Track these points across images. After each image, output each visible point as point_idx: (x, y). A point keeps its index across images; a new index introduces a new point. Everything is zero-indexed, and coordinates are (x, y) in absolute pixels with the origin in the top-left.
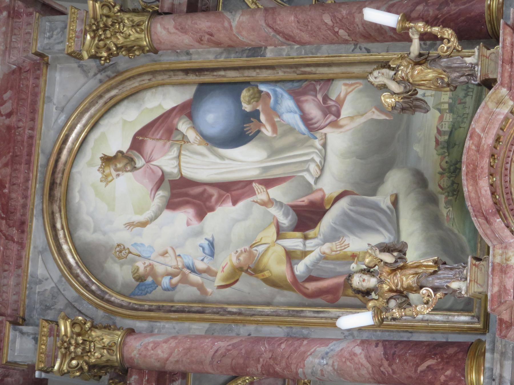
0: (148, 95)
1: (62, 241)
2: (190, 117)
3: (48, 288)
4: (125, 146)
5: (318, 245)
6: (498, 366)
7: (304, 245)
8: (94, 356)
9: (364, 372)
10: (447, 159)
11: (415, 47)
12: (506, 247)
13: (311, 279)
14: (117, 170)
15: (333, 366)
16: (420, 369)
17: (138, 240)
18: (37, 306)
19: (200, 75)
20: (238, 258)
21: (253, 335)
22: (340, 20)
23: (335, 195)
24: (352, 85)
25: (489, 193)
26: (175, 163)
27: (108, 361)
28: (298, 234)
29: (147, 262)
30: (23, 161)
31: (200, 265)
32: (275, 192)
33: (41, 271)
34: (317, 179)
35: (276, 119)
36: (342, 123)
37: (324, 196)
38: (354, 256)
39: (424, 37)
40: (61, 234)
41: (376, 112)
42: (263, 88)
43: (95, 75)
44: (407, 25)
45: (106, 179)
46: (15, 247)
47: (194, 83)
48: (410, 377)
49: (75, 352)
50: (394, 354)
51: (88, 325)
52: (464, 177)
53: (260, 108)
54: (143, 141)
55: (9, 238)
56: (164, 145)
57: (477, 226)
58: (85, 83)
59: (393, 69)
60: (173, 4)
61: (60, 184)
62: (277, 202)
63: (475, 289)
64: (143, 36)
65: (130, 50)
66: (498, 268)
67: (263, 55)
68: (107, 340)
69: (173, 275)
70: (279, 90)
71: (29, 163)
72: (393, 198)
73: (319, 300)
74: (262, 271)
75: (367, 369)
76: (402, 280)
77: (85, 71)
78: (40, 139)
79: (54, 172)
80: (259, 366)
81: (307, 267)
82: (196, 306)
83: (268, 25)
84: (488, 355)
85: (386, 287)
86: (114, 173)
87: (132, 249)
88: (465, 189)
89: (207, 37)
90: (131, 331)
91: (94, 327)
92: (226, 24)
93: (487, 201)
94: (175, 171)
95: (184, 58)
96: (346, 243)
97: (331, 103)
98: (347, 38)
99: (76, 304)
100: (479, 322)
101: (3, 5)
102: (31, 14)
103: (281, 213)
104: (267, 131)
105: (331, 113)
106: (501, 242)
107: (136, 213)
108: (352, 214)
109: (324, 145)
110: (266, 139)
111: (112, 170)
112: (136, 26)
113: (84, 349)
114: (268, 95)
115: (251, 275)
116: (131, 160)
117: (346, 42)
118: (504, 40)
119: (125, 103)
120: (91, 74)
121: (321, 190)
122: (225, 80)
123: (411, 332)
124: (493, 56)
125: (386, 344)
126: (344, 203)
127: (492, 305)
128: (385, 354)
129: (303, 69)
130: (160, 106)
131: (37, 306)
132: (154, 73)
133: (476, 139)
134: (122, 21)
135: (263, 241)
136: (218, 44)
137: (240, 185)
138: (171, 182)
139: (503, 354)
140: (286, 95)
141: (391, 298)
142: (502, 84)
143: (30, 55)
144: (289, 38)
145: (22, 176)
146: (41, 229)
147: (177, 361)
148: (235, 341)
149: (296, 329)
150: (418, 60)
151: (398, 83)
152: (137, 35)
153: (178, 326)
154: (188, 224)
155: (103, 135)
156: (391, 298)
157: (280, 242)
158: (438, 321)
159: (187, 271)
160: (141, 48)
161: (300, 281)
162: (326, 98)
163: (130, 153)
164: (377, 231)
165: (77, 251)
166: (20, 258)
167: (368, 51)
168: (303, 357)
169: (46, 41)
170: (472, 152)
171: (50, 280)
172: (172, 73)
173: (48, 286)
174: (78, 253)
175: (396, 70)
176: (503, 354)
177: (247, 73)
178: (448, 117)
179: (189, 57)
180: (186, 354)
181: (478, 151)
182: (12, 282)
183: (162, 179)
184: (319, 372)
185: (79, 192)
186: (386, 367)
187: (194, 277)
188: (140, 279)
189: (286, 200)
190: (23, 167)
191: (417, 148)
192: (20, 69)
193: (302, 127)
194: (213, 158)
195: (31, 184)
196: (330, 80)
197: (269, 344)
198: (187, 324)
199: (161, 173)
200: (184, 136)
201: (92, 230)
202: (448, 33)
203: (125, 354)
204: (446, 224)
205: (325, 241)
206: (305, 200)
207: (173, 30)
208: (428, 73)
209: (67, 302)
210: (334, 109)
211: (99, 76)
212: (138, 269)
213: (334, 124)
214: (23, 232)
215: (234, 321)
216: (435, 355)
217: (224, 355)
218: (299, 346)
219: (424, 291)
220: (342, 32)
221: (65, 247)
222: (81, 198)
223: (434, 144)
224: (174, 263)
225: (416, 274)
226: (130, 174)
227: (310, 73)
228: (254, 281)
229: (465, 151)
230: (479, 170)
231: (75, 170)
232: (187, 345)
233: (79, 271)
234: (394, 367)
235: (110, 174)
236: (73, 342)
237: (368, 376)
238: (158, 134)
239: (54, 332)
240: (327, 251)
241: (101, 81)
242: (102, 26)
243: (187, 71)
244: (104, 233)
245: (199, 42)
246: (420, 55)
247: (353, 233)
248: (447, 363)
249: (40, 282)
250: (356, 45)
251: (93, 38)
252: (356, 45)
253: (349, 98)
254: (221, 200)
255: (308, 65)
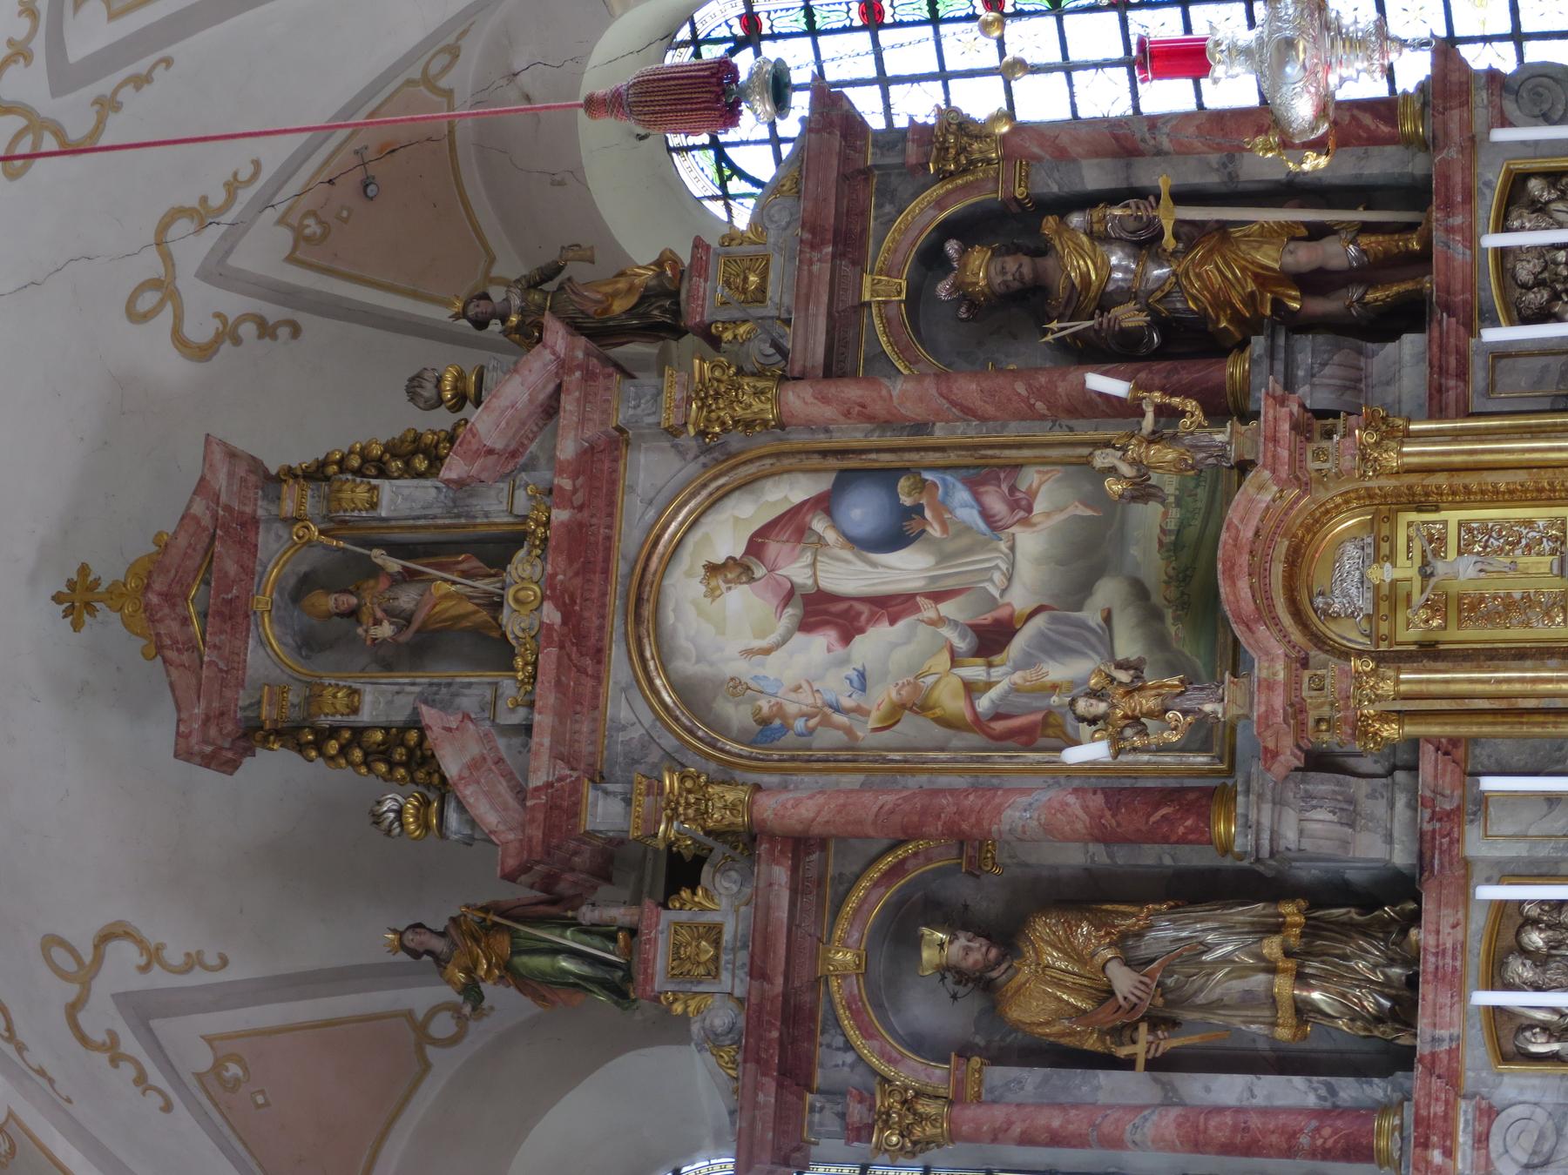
0: (768, 484)
1: (654, 674)
2: (829, 512)
3: (636, 735)
4: (738, 551)
5: (1006, 674)
6: (1255, 810)
7: (989, 674)
8: (711, 818)
9: (1079, 826)
10: (1173, 564)
11: (1148, 422)
12: (1272, 660)
13: (998, 716)
14: (727, 581)
15: (1038, 820)
16: (1152, 819)
17: (760, 672)
18: (621, 759)
19: (843, 459)
20: (898, 693)
21: (925, 787)
22: (1038, 390)
23: (1028, 611)
24: (1047, 472)
25: (1250, 595)
26: (809, 572)
27: (729, 825)
28: (980, 660)
29: (773, 701)
30: (598, 569)
31: (847, 702)
32: (947, 608)
33: (624, 714)
34: (1003, 592)
35: (947, 516)
36: (1035, 520)
37: (1013, 611)
38: (1055, 687)
39: (1160, 410)
40: (651, 664)
41: (1080, 507)
42: (928, 476)
43: (696, 457)
44: (1141, 394)
45: (712, 593)
46: (590, 683)
47: (833, 470)
48: (1139, 830)
49: (685, 814)
50: (1119, 801)
51: (703, 779)
52: (1220, 577)
53: (923, 501)
54: (763, 545)
55: (582, 671)
56: (793, 549)
57: (1238, 634)
58: (680, 471)
59: (1119, 449)
60: (804, 367)
61: (648, 600)
62: (949, 620)
63: (1234, 711)
64: (769, 406)
65: (748, 425)
66: (1264, 684)
67: (931, 434)
68: (730, 797)
69: (809, 716)
70: (949, 478)
71: (606, 572)
72: (1105, 614)
73: (1009, 743)
74: (932, 708)
75: (1084, 822)
76: (1141, 704)
77: (681, 452)
78: (619, 540)
79: (641, 585)
80: (940, 824)
81: (993, 701)
82: (844, 755)
83: (941, 395)
84: (1240, 799)
85: (1119, 713)
86: (723, 586)
87: (752, 684)
88: (1222, 590)
89: (857, 409)
90: (757, 788)
91: (709, 782)
92: (884, 392)
93: (1247, 606)
94: (810, 582)
95: (822, 436)
96: (1044, 670)
97: (1019, 495)
98: (1046, 412)
99: (677, 756)
100: (1222, 762)
101: (575, 363)
102: (610, 376)
103: (956, 634)
104: (935, 531)
105: (1020, 507)
106: (1267, 653)
107: (756, 637)
108: (1050, 634)
109: (1012, 549)
110: (933, 541)
111: (721, 582)
112: (758, 393)
113: (697, 810)
114: (935, 484)
115: (917, 713)
116: (747, 569)
117: (1042, 417)
118: (1266, 413)
119: (737, 494)
120: (690, 456)
121: (1009, 604)
122: (877, 465)
123: (1135, 778)
124: (1249, 434)
125: (1108, 793)
126: (1040, 621)
127: (1259, 727)
128: (1107, 802)
129: (983, 452)
130: (786, 498)
131: (621, 759)
132: (778, 455)
133: (1234, 531)
134: (740, 387)
135: (932, 671)
136: (870, 419)
137: (899, 601)
138: (803, 596)
139: (1260, 796)
140: (959, 485)
141: (1127, 726)
142: (1264, 466)
143: (610, 429)
144: (968, 412)
145: (597, 589)
146: (625, 659)
147: (827, 822)
148: (904, 794)
149: (983, 779)
150: (1152, 437)
151: (1131, 464)
152: (761, 406)
153: (823, 779)
154: (829, 650)
155: (706, 537)
156: (1127, 726)
157: (955, 671)
158: (1169, 764)
159: (829, 711)
160: (765, 423)
161: (982, 719)
162: (1013, 489)
163: (745, 559)
164: (1083, 654)
165: (674, 686)
166: (596, 696)
167: (1071, 429)
168: (999, 810)
169: (631, 412)
170: (1227, 547)
171: (638, 725)
172: (804, 456)
173: (636, 733)
174: (674, 690)
175: (1124, 449)
176: (1260, 796)
177: (907, 456)
178: (1175, 513)
179: (828, 435)
180: (839, 812)
181: (1235, 545)
182: (585, 728)
183: (791, 594)
184: (1020, 829)
185: (674, 610)
186: (1109, 820)
187: (839, 718)
188: (764, 722)
189: (962, 618)
190: (597, 578)
191: (1134, 551)
192: (592, 448)
193: (982, 525)
194: (860, 566)
195: (610, 599)
196: (1017, 467)
197: (952, 795)
198: (834, 777)
199: (789, 585)
200: (820, 538)
201: (694, 659)
202: (1191, 405)
203: (755, 814)
204: (1175, 645)
205: (1016, 669)
206: (988, 618)
207: (812, 400)
208: (1167, 454)
209: (662, 753)
210: (1024, 503)
211: (702, 459)
212: (760, 709)
213: (1025, 522)
214: (599, 662)
215: (900, 771)
216: (1172, 801)
217: (892, 812)
218: (993, 797)
219: (1170, 714)
220: (1039, 405)
221: (658, 682)
222: (677, 618)
223: (1157, 546)
224: (810, 700)
225: (1159, 695)
226: (746, 586)
227: (992, 457)
228: (920, 721)
229: (1221, 545)
230: (1237, 569)
231: (666, 582)
232: (841, 801)
233: (678, 713)
234: (1119, 817)
235: (718, 587)
236: (682, 801)
237: (1084, 831)
238: (446, 610)
239: (656, 788)
240: (1019, 681)
241: (705, 465)
242: (712, 393)
243: (825, 453)
244: (712, 664)
245: (845, 416)
246: (1154, 432)
247: (1053, 658)
248: (1188, 810)
249: (624, 728)
250: (1054, 422)
251: (700, 409)
252: (1054, 422)
253: (1043, 488)
254: (873, 619)
255: (992, 447)
